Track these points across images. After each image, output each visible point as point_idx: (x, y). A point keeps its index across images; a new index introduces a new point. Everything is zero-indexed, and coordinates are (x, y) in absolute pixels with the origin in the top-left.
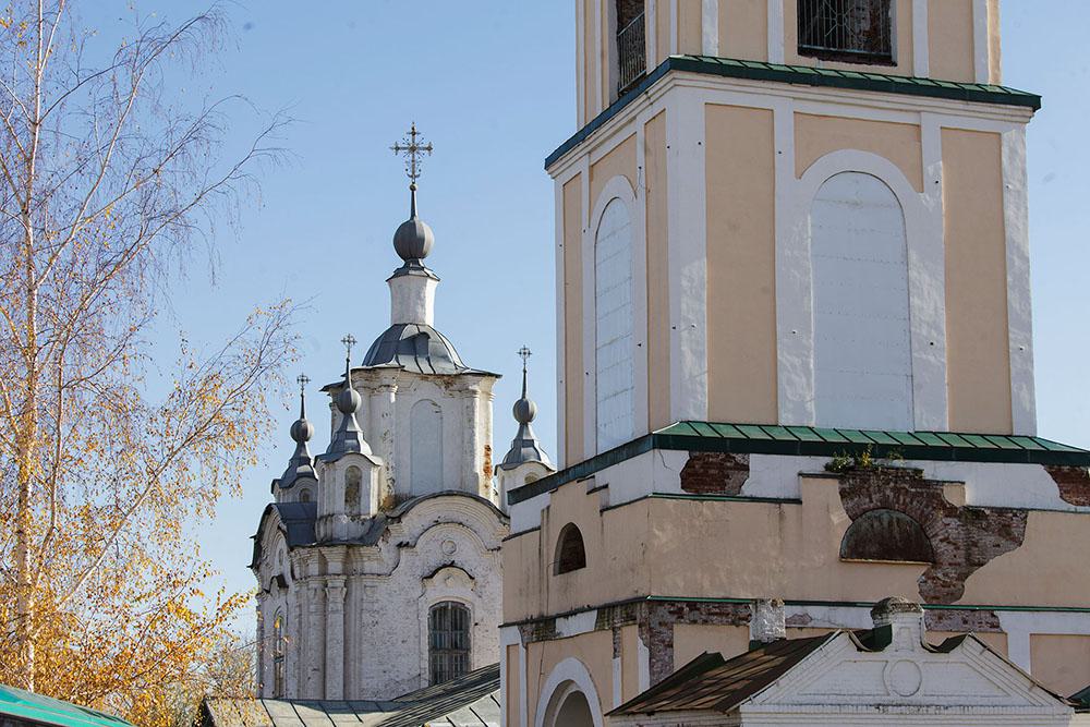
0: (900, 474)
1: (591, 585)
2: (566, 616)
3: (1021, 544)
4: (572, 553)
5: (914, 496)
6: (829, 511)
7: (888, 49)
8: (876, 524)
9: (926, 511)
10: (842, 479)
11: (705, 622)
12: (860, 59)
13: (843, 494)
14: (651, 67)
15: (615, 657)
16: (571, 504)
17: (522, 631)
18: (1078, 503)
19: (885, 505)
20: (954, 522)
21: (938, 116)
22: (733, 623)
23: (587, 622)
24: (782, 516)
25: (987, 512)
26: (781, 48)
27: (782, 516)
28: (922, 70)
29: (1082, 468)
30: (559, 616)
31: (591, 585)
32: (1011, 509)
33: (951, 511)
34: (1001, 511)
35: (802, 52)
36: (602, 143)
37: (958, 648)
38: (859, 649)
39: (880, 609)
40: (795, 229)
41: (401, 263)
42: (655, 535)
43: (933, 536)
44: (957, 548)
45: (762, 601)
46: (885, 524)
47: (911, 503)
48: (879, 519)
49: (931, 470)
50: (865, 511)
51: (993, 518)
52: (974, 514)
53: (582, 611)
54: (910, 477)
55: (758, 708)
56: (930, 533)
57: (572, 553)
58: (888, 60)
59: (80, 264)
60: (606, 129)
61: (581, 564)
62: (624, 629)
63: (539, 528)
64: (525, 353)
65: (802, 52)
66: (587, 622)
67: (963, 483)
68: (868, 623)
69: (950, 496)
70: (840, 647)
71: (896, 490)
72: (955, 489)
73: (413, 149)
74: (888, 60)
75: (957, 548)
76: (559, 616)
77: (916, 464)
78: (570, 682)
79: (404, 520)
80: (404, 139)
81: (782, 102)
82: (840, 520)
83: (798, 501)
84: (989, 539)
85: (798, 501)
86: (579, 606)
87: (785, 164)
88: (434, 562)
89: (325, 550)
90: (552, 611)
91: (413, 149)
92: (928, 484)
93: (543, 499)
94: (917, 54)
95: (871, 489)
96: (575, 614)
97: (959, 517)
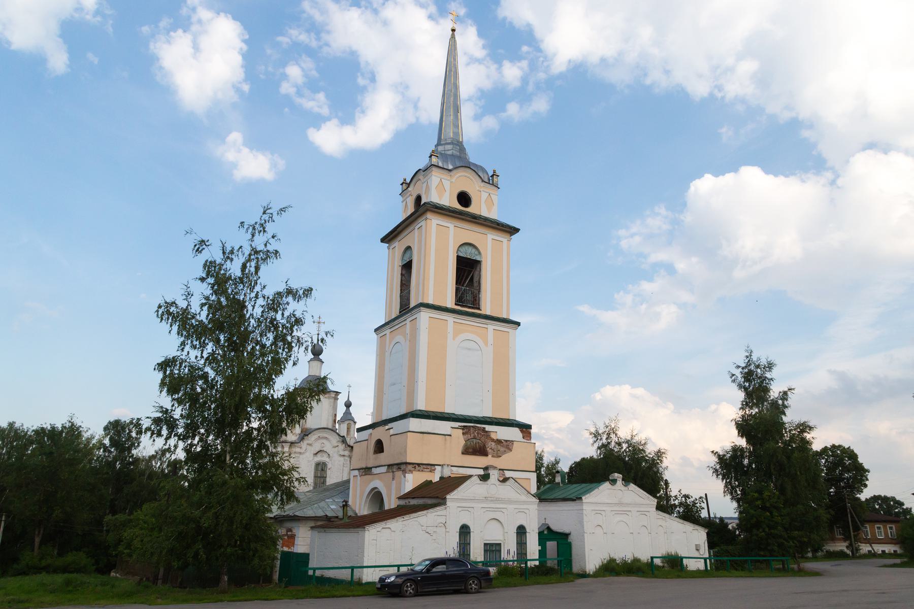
0: (479, 428)
1: (384, 458)
2: (376, 467)
4: (379, 447)
5: (483, 435)
6: (459, 439)
7: (479, 305)
8: (472, 443)
9: (486, 440)
10: (463, 429)
11: (422, 471)
12: (469, 307)
13: (463, 434)
14: (412, 304)
15: (393, 480)
16: (379, 433)
17: (359, 472)
18: (527, 440)
19: (475, 438)
20: (493, 443)
21: (492, 326)
22: (430, 471)
23: (384, 469)
24: (445, 439)
26: (450, 302)
27: (445, 439)
28: (488, 313)
30: (373, 467)
31: (384, 458)
32: (509, 441)
33: (493, 440)
34: (506, 441)
35: (456, 304)
36: (395, 326)
38: (481, 480)
39: (486, 469)
41: (313, 357)
42: (753, 388)
44: (494, 451)
45: (445, 465)
46: (474, 443)
49: (488, 428)
50: (469, 439)
51: (504, 443)
52: (499, 442)
53: (382, 466)
55: (451, 497)
56: (487, 447)
57: (379, 447)
58: (479, 309)
60: (396, 322)
61: (382, 451)
62: (396, 473)
63: (367, 440)
64: (349, 386)
65: (456, 304)
66: (384, 469)
68: (481, 472)
69: (493, 436)
70: (475, 480)
71: (478, 433)
72: (494, 434)
73: (319, 323)
74: (479, 309)
75: (494, 451)
76: (373, 467)
78: (376, 488)
79: (309, 435)
80: (322, 320)
81: (450, 318)
82: (462, 442)
83: (450, 435)
84: (502, 449)
85: (450, 435)
86: (381, 465)
87: (450, 336)
88: (318, 450)
89: (284, 444)
90: (370, 466)
91: (319, 323)
93: (370, 431)
94: (487, 308)
97: (495, 442)
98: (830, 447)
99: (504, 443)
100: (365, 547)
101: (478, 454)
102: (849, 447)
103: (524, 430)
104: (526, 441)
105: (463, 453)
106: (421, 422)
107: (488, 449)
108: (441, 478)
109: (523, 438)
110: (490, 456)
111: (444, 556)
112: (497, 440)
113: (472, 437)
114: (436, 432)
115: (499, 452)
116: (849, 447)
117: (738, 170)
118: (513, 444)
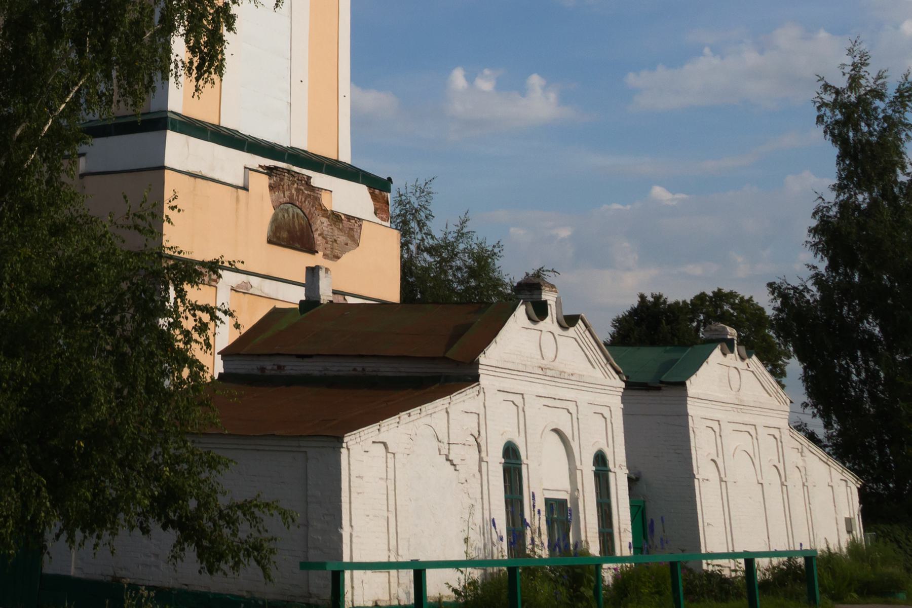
3: (358, 245)
8: (286, 215)
13: (272, 188)
18: (382, 219)
20: (324, 220)
25: (343, 217)
29: (385, 193)
33: (325, 212)
34: (349, 218)
37: (655, 523)
40: (72, 370)
43: (143, 229)
46: (291, 216)
47: (305, 202)
48: (287, 211)
49: (319, 180)
51: (345, 222)
54: (305, 181)
59: (139, 221)
67: (331, 191)
71: (298, 190)
77: (306, 172)
92: (313, 189)
95: (285, 186)
96: (196, 177)
97: (328, 218)
98: (711, 295)
99: (345, 222)
100: (343, 500)
101: (298, 246)
102: (751, 299)
103: (377, 191)
104: (379, 221)
105: (270, 242)
106: (188, 143)
107: (316, 235)
108: (546, 301)
109: (375, 213)
110: (321, 254)
111: (428, 594)
112: (333, 212)
113: (287, 199)
114: (216, 177)
115: (335, 244)
116: (751, 299)
117: (675, 303)
118: (360, 226)
